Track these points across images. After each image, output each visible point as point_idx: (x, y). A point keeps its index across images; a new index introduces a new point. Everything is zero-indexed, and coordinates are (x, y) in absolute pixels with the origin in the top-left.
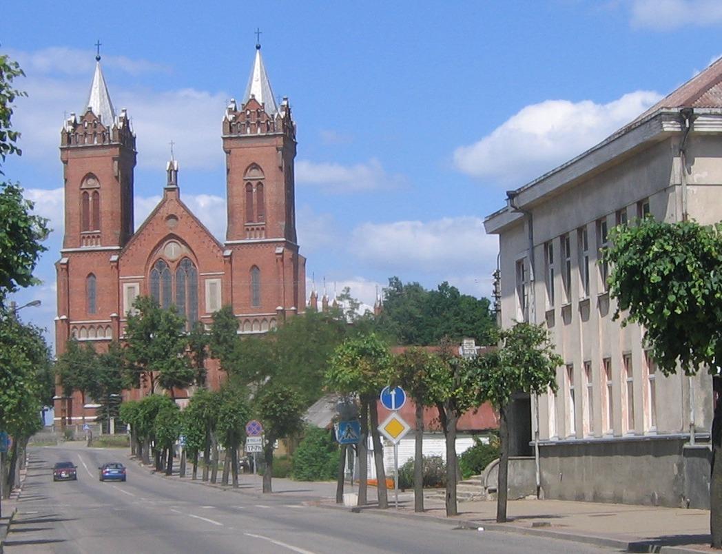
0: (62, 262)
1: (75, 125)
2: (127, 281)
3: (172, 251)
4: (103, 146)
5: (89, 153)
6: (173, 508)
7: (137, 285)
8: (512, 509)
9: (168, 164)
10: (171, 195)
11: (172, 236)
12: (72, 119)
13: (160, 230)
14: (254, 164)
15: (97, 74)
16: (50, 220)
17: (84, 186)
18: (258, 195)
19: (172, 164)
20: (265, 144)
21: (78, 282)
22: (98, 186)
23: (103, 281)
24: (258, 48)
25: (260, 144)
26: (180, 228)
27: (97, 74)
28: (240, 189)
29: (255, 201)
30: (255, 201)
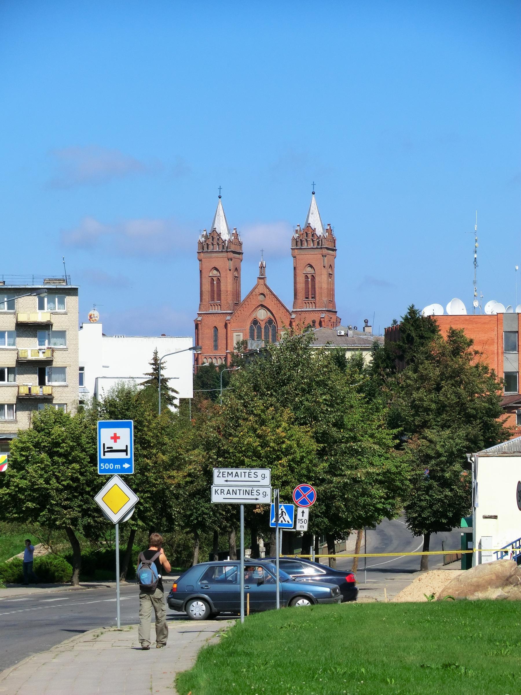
0: (198, 320)
1: (206, 237)
2: (236, 331)
3: (262, 315)
4: (222, 251)
5: (214, 255)
6: (504, 653)
7: (241, 334)
8: (32, 280)
9: (260, 263)
10: (261, 281)
11: (262, 306)
12: (205, 233)
13: (255, 303)
14: (309, 264)
15: (220, 207)
16: (413, 306)
17: (211, 275)
18: (312, 283)
19: (262, 263)
20: (316, 253)
21: (207, 333)
22: (219, 275)
23: (222, 331)
24: (313, 193)
25: (313, 253)
26: (269, 303)
27: (220, 207)
28: (301, 279)
29: (215, 289)
30: (215, 289)
